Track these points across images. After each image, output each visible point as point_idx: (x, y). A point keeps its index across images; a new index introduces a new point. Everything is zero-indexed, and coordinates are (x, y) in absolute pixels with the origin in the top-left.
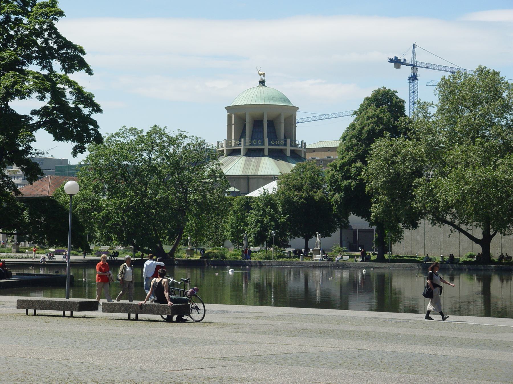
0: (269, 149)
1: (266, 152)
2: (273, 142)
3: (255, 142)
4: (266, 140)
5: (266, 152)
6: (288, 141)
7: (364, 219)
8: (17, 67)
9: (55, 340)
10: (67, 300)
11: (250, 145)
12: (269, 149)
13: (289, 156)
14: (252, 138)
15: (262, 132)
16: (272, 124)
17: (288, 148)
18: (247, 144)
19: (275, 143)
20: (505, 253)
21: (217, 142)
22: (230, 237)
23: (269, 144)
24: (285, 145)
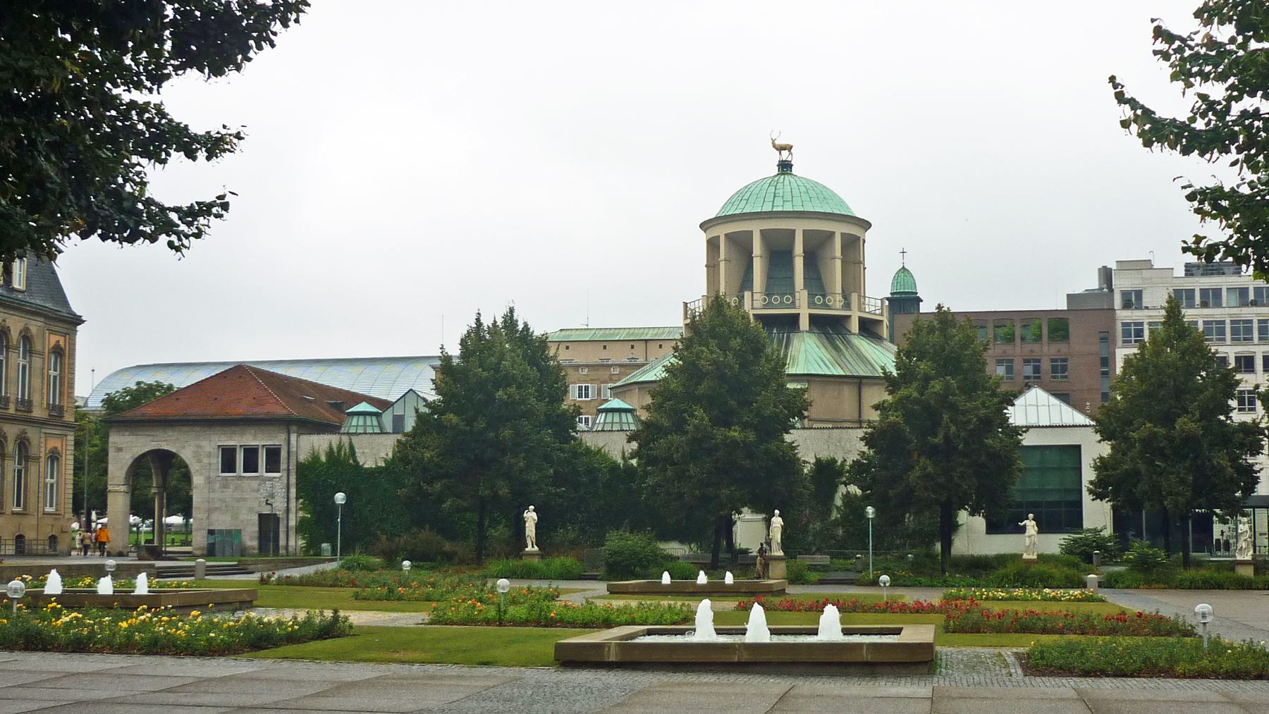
0: (811, 316)
1: (804, 323)
2: (818, 299)
3: (776, 300)
4: (802, 296)
5: (804, 323)
6: (854, 297)
7: (94, 238)
8: (1254, 131)
9: (830, 449)
10: (1084, 489)
11: (765, 307)
12: (811, 316)
13: (857, 331)
14: (768, 292)
15: (791, 278)
16: (816, 249)
17: (855, 315)
18: (757, 304)
19: (782, 302)
20: (132, 93)
21: (682, 305)
22: (798, 425)
23: (811, 304)
24: (847, 306)
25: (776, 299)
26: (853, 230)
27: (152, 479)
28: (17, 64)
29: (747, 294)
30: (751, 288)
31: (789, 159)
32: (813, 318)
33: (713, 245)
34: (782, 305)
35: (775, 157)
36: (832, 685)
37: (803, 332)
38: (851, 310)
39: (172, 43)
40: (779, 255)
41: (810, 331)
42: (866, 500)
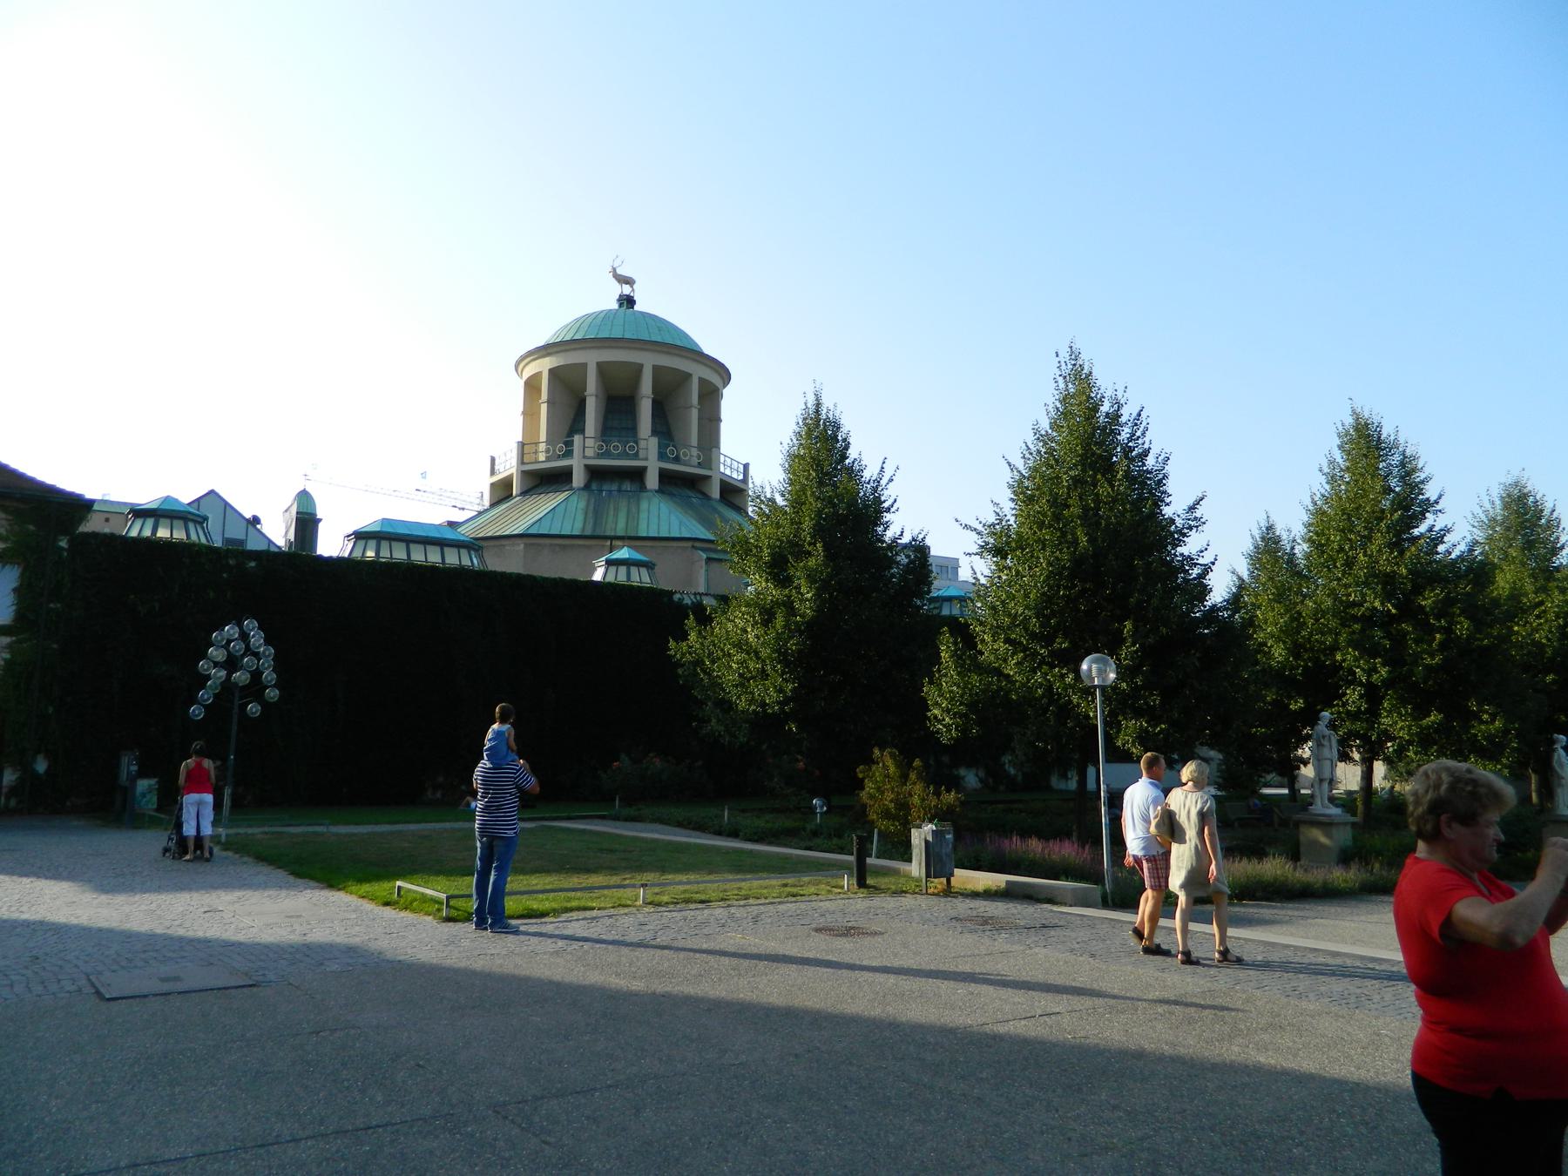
1: (652, 480)
5: (652, 480)
11: (599, 456)
14: (606, 431)
18: (589, 452)
23: (662, 456)
25: (616, 445)
26: (715, 379)
27: (615, 800)
28: (596, 1160)
29: (577, 439)
30: (582, 431)
31: (632, 294)
32: (666, 478)
33: (531, 386)
34: (625, 455)
35: (617, 290)
36: (853, 1010)
37: (651, 491)
38: (711, 469)
39: (208, 758)
40: (619, 406)
41: (660, 491)
42: (266, 705)
